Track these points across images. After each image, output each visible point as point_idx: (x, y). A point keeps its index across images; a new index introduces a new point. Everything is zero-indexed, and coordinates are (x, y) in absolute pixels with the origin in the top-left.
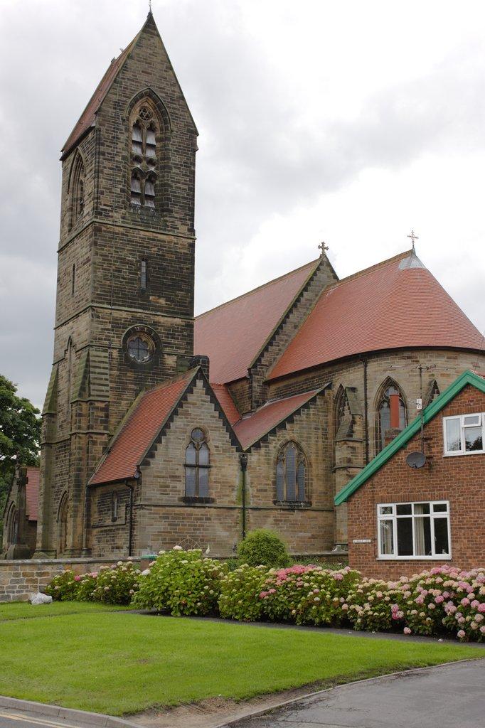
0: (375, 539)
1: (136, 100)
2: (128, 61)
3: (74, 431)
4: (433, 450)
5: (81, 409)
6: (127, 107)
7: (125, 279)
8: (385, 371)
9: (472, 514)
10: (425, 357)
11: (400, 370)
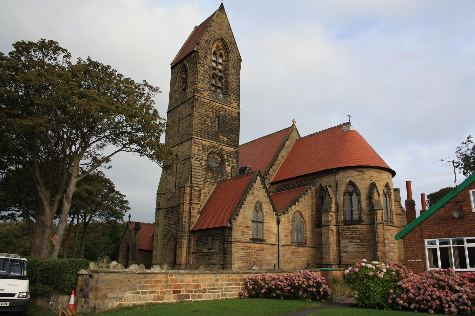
0: (424, 260)
1: (215, 41)
3: (181, 202)
6: (211, 43)
7: (208, 125)
8: (348, 177)
10: (368, 171)
11: (355, 176)
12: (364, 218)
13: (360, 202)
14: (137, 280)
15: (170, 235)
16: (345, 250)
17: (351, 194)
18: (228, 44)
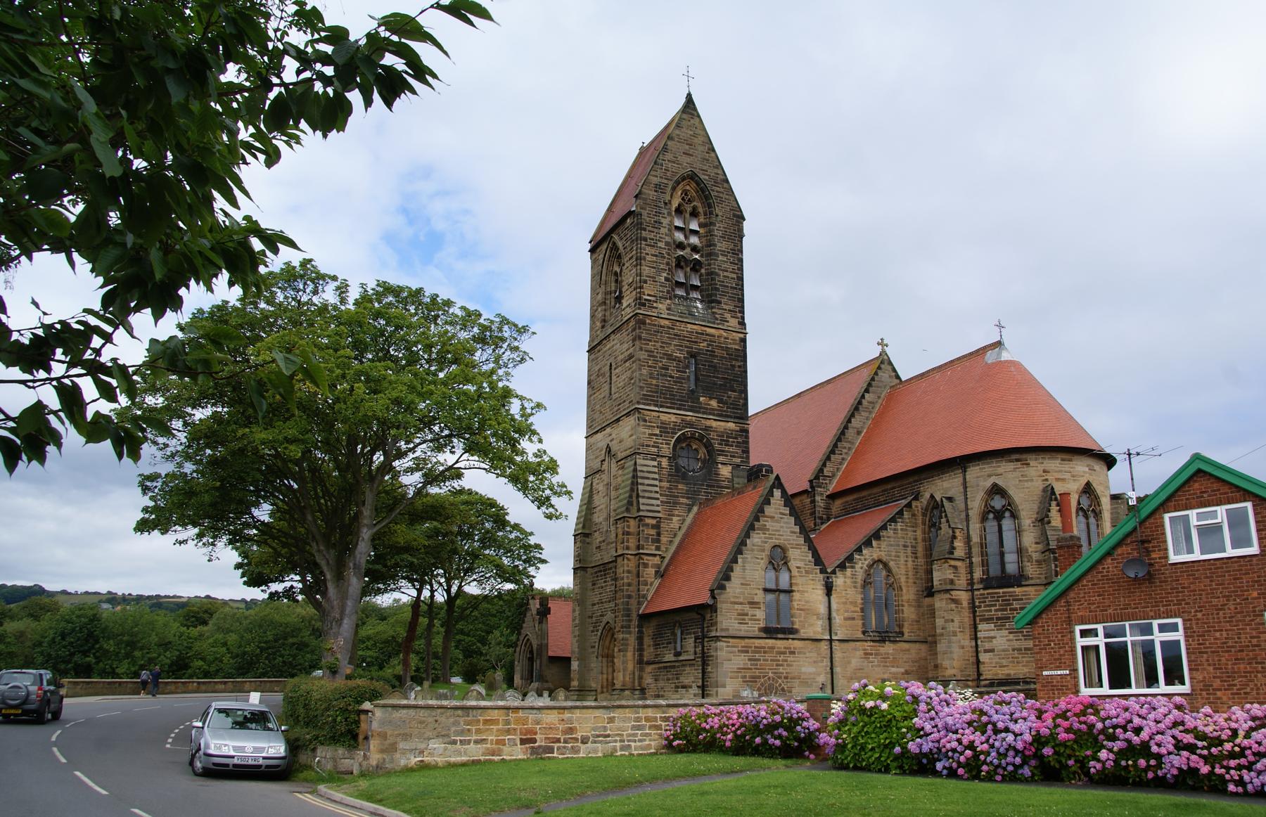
0: (1076, 670)
1: (678, 183)
2: (669, 143)
3: (620, 552)
4: (1153, 556)
5: (628, 527)
6: (669, 190)
8: (990, 476)
9: (1218, 634)
11: (1005, 474)
12: (1030, 570)
13: (1019, 532)
14: (452, 720)
15: (603, 625)
16: (987, 646)
17: (999, 516)
18: (709, 184)
